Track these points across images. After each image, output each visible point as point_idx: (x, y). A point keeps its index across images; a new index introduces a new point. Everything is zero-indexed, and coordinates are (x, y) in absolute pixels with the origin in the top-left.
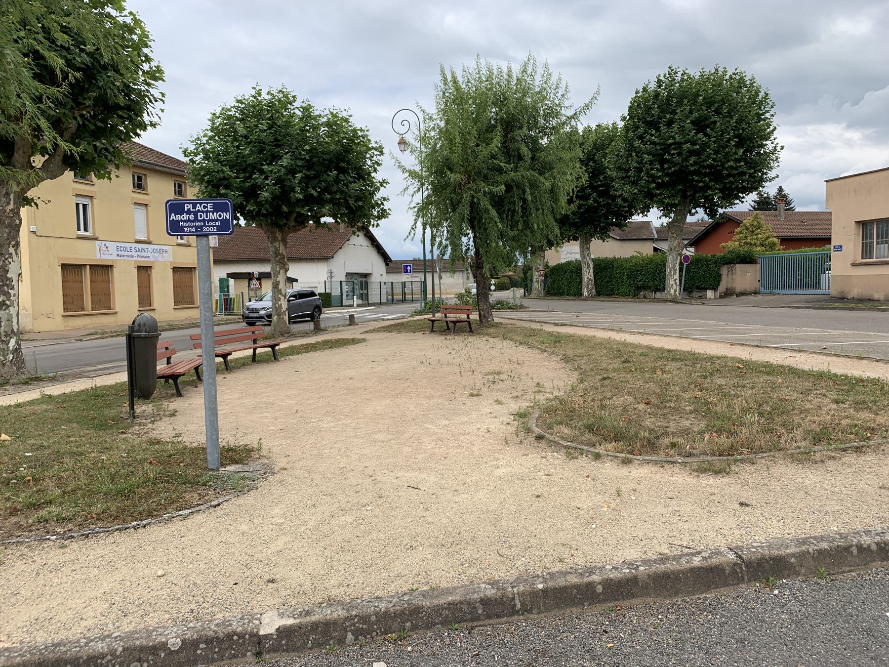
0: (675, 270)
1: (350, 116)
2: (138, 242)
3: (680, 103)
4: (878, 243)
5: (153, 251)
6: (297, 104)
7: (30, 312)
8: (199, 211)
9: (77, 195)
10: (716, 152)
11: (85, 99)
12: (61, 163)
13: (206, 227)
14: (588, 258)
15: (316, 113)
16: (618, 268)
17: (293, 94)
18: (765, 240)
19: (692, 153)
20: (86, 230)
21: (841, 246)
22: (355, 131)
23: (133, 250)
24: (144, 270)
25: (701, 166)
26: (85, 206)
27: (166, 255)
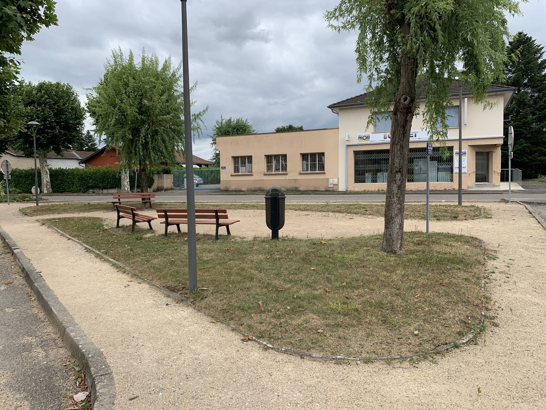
4: (241, 167)
14: (46, 168)
21: (225, 167)
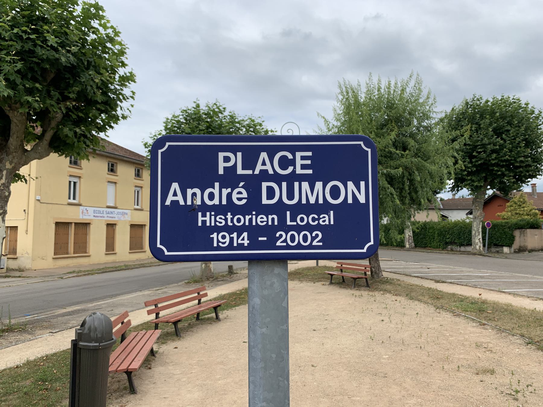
0: (479, 232)
1: (263, 122)
2: (108, 207)
3: (482, 117)
5: (118, 213)
6: (226, 113)
7: (30, 255)
8: (264, 176)
9: (71, 176)
10: (511, 151)
11: (70, 93)
12: (47, 147)
13: (287, 229)
15: (240, 119)
16: (430, 228)
17: (224, 106)
18: (529, 212)
19: (493, 151)
20: (74, 199)
22: (267, 132)
23: (105, 213)
24: (111, 226)
25: (499, 160)
26: (75, 183)
27: (126, 216)
